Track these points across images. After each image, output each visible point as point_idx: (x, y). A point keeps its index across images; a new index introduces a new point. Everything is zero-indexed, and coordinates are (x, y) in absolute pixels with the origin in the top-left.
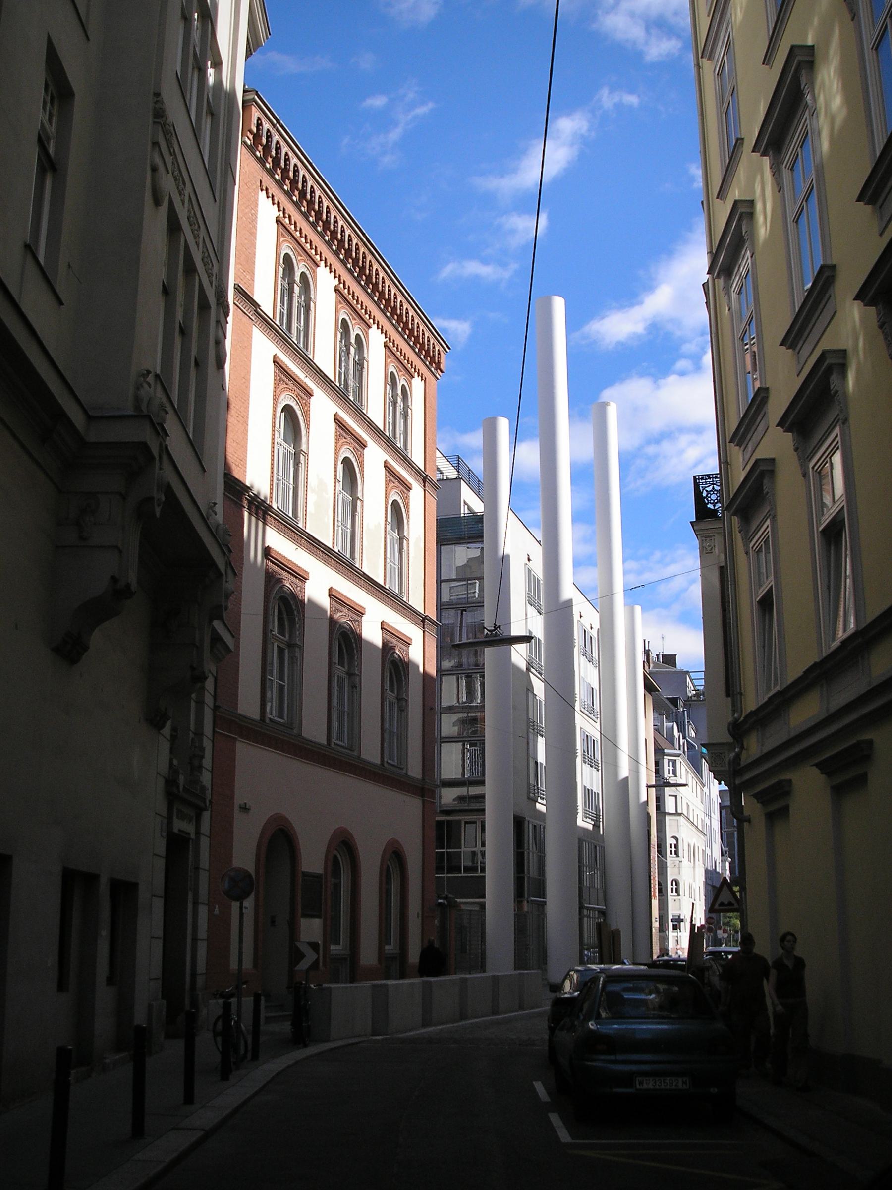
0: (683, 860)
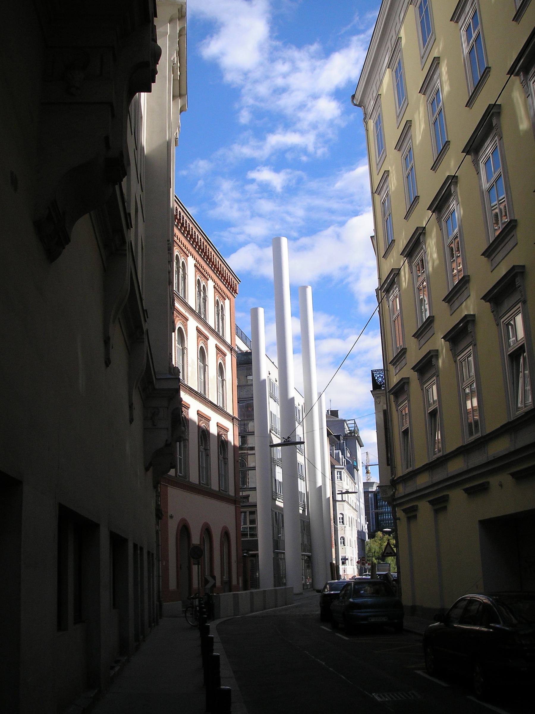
0: (346, 526)
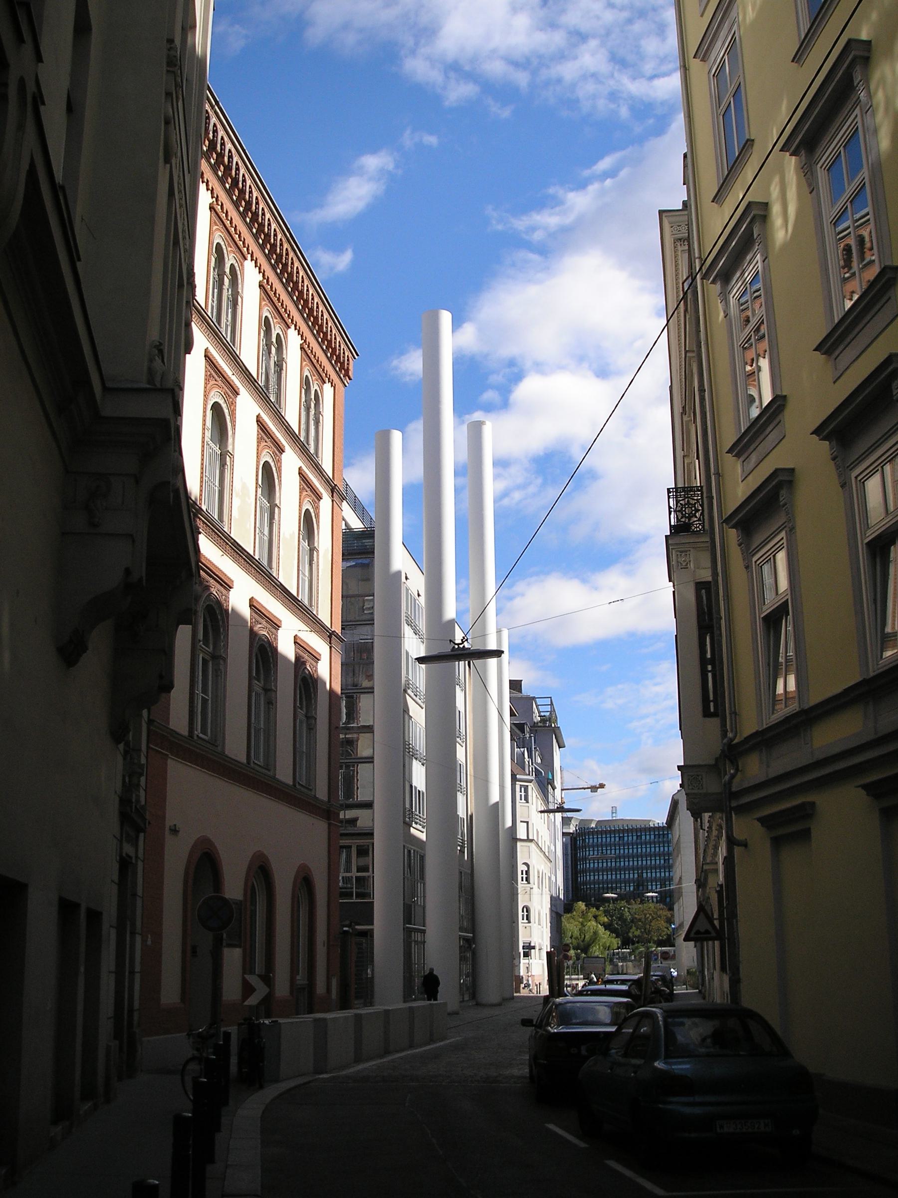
0: (534, 886)
